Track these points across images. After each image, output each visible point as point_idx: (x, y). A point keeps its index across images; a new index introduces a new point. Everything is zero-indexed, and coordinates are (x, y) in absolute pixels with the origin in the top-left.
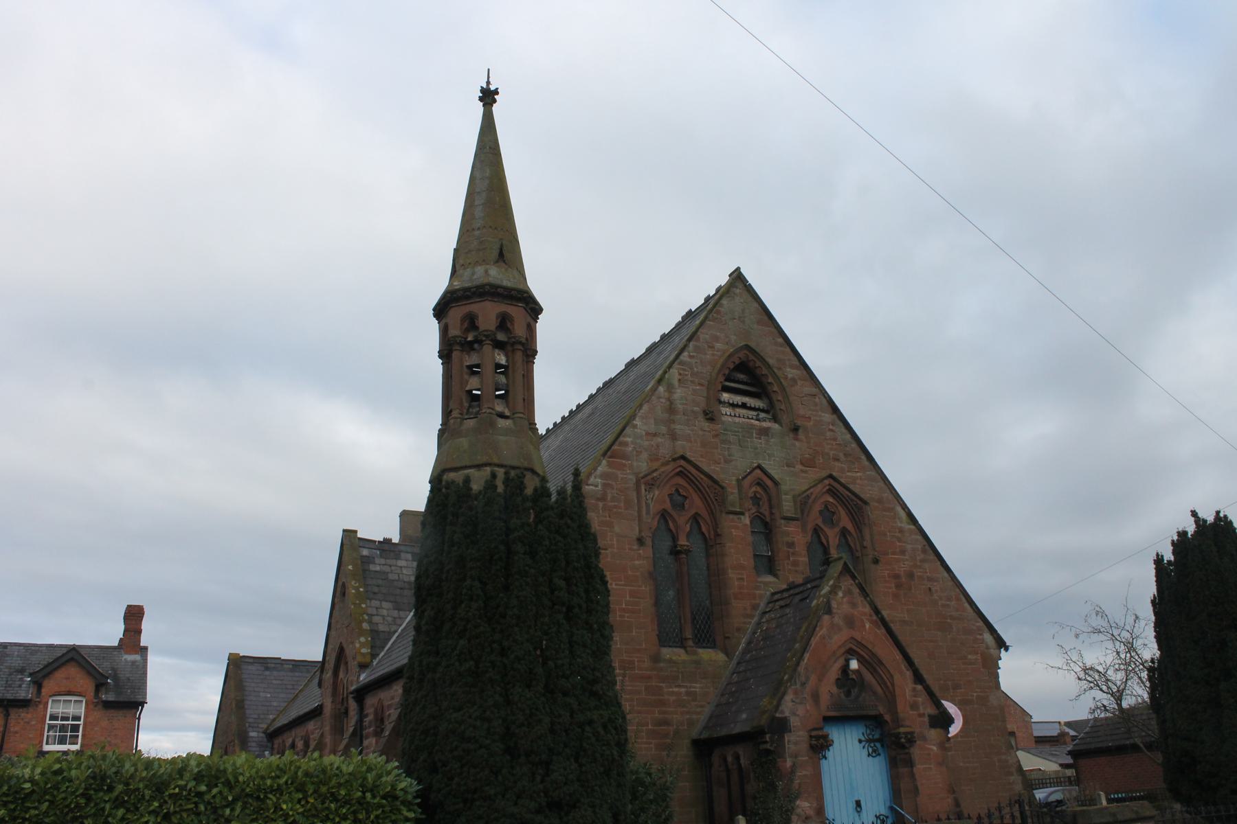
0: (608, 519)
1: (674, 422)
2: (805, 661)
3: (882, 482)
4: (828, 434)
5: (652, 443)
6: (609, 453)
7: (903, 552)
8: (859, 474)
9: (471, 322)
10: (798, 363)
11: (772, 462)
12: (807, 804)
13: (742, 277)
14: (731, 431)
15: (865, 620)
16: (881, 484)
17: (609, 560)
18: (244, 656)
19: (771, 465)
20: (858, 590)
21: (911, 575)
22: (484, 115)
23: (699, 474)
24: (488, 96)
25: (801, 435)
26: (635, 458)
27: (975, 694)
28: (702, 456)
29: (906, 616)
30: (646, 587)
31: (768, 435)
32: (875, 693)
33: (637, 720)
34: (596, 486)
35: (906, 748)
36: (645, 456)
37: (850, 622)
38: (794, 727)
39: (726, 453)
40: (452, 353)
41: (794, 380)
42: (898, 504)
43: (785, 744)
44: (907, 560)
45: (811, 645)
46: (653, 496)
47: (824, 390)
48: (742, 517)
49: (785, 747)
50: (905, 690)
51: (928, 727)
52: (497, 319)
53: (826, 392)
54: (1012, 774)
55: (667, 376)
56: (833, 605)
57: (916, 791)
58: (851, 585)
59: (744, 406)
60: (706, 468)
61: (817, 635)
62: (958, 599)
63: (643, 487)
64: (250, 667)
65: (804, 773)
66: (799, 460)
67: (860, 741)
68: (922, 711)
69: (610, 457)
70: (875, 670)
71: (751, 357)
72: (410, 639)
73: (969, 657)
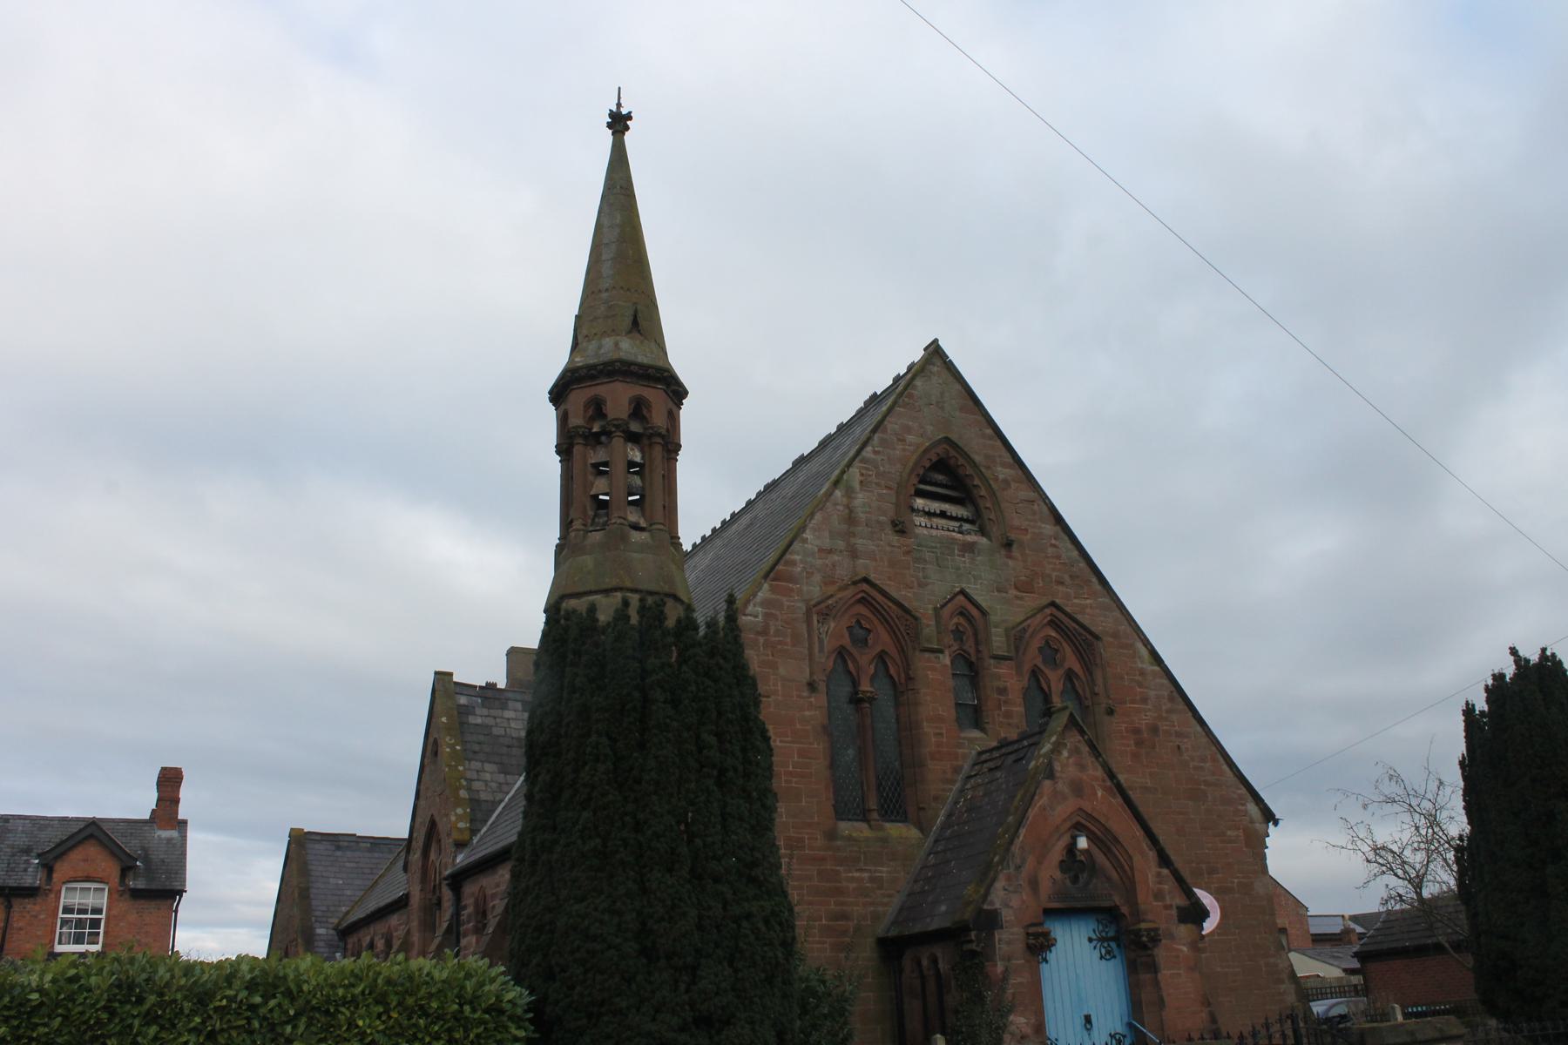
0: (771, 658)
1: (854, 535)
2: (1021, 838)
3: (1119, 611)
4: (1050, 550)
5: (827, 562)
6: (772, 575)
7: (1145, 700)
8: (1088, 601)
9: (597, 408)
10: (1011, 461)
11: (978, 587)
12: (1023, 1020)
13: (940, 351)
14: (926, 547)
15: (1096, 786)
16: (1117, 614)
17: (772, 710)
18: (309, 832)
19: (977, 589)
20: (1087, 749)
21: (1154, 730)
22: (614, 146)
23: (886, 601)
24: (619, 122)
25: (1016, 552)
26: (805, 581)
27: (1236, 881)
28: (890, 579)
29: (1148, 781)
30: (819, 744)
31: (973, 552)
32: (1109, 879)
33: (807, 913)
34: (756, 617)
35: (1149, 949)
36: (817, 578)
37: (1078, 788)
38: (1006, 921)
39: (921, 574)
41: (1006, 482)
42: (1138, 639)
43: (995, 943)
44: (1150, 710)
45: (1028, 818)
46: (828, 629)
47: (1045, 494)
48: (941, 656)
49: (995, 947)
50: (1147, 875)
51: (1176, 921)
53: (1047, 497)
54: (1282, 982)
55: (845, 477)
56: (1056, 768)
57: (1161, 1003)
58: (1079, 742)
59: (943, 515)
60: (894, 594)
61: (1035, 805)
62: (1214, 760)
63: (815, 618)
64: (317, 846)
65: (1019, 980)
66: (1013, 583)
67: (1090, 940)
68: (1168, 902)
69: (773, 580)
70: (1109, 850)
71: (953, 453)
73: (1229, 833)
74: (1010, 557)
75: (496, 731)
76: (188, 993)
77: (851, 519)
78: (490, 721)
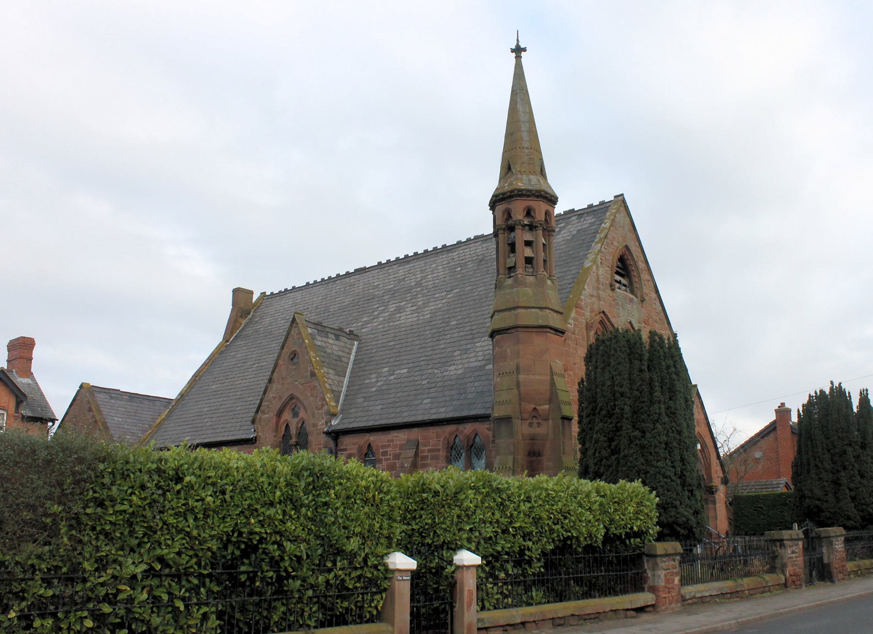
18: (93, 386)
24: (518, 51)
40: (680, 541)
52: (524, 211)
57: (716, 518)
64: (99, 395)
74: (642, 307)
75: (329, 351)
78: (324, 345)
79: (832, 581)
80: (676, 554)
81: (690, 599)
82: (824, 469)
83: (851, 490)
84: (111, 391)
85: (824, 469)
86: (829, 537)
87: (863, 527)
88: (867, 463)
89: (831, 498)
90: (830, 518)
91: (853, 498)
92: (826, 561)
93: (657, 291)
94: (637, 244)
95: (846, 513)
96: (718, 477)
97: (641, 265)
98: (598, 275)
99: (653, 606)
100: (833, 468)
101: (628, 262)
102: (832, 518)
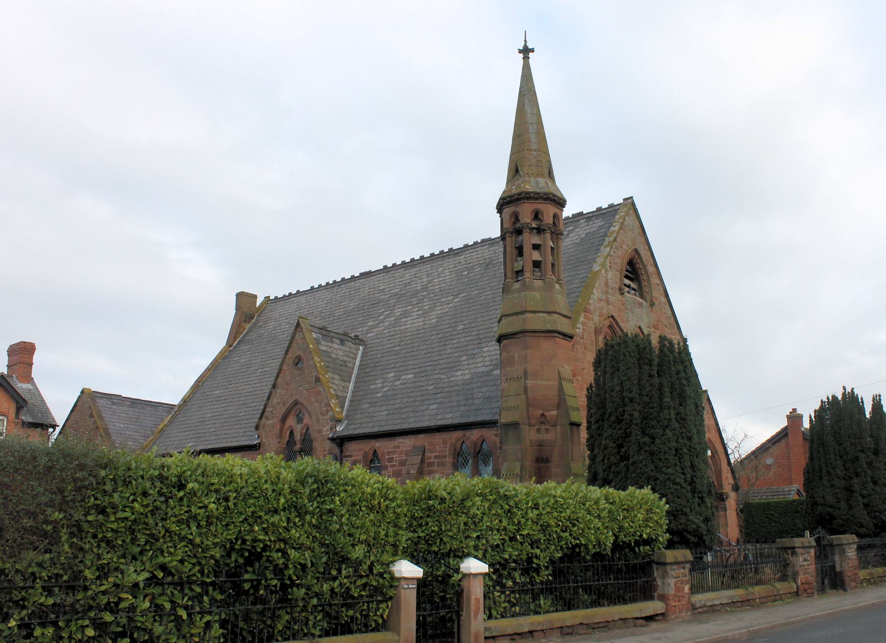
18: (94, 392)
24: (526, 51)
40: (690, 549)
57: (727, 525)
64: (101, 401)
72: (269, 383)
75: (334, 356)
76: (664, 499)
77: (607, 285)
79: (845, 590)
80: (686, 562)
81: (700, 608)
82: (836, 475)
83: (863, 497)
84: (113, 397)
85: (836, 475)
86: (841, 545)
87: (876, 535)
88: (880, 470)
89: (843, 505)
90: (842, 526)
91: (866, 505)
92: (838, 569)
93: (667, 295)
94: (647, 247)
95: (859, 520)
96: (729, 484)
97: (651, 269)
98: (607, 279)
99: (663, 614)
100: (845, 474)
101: (637, 266)
102: (844, 526)
